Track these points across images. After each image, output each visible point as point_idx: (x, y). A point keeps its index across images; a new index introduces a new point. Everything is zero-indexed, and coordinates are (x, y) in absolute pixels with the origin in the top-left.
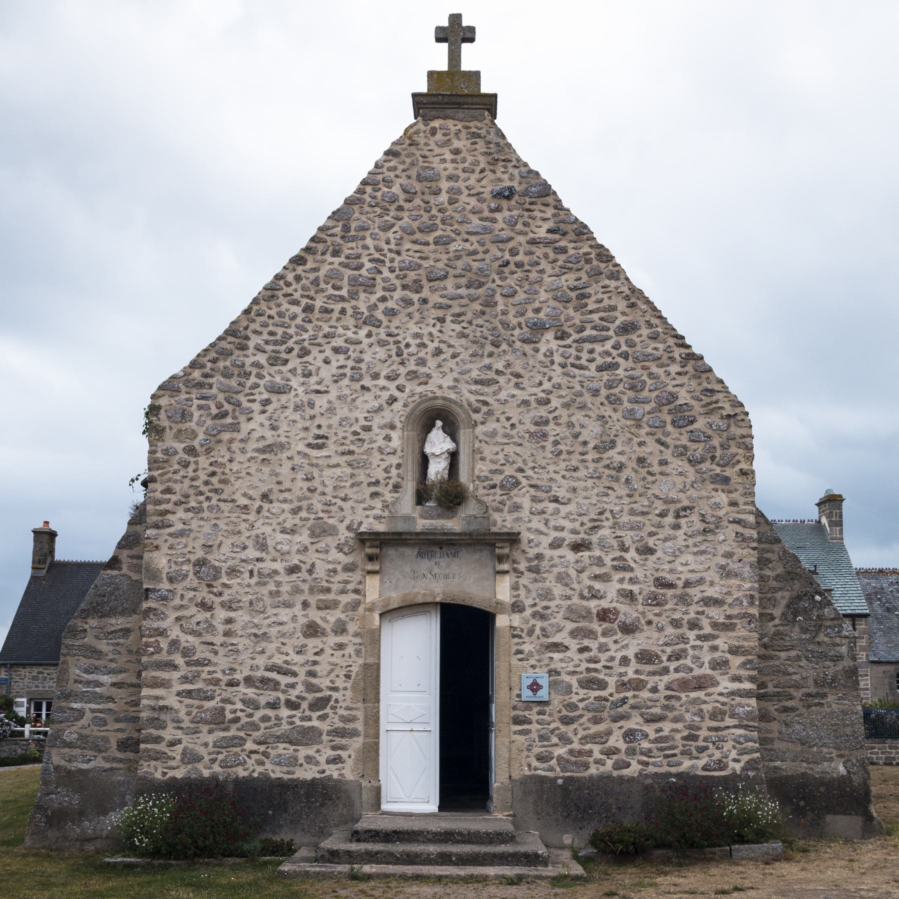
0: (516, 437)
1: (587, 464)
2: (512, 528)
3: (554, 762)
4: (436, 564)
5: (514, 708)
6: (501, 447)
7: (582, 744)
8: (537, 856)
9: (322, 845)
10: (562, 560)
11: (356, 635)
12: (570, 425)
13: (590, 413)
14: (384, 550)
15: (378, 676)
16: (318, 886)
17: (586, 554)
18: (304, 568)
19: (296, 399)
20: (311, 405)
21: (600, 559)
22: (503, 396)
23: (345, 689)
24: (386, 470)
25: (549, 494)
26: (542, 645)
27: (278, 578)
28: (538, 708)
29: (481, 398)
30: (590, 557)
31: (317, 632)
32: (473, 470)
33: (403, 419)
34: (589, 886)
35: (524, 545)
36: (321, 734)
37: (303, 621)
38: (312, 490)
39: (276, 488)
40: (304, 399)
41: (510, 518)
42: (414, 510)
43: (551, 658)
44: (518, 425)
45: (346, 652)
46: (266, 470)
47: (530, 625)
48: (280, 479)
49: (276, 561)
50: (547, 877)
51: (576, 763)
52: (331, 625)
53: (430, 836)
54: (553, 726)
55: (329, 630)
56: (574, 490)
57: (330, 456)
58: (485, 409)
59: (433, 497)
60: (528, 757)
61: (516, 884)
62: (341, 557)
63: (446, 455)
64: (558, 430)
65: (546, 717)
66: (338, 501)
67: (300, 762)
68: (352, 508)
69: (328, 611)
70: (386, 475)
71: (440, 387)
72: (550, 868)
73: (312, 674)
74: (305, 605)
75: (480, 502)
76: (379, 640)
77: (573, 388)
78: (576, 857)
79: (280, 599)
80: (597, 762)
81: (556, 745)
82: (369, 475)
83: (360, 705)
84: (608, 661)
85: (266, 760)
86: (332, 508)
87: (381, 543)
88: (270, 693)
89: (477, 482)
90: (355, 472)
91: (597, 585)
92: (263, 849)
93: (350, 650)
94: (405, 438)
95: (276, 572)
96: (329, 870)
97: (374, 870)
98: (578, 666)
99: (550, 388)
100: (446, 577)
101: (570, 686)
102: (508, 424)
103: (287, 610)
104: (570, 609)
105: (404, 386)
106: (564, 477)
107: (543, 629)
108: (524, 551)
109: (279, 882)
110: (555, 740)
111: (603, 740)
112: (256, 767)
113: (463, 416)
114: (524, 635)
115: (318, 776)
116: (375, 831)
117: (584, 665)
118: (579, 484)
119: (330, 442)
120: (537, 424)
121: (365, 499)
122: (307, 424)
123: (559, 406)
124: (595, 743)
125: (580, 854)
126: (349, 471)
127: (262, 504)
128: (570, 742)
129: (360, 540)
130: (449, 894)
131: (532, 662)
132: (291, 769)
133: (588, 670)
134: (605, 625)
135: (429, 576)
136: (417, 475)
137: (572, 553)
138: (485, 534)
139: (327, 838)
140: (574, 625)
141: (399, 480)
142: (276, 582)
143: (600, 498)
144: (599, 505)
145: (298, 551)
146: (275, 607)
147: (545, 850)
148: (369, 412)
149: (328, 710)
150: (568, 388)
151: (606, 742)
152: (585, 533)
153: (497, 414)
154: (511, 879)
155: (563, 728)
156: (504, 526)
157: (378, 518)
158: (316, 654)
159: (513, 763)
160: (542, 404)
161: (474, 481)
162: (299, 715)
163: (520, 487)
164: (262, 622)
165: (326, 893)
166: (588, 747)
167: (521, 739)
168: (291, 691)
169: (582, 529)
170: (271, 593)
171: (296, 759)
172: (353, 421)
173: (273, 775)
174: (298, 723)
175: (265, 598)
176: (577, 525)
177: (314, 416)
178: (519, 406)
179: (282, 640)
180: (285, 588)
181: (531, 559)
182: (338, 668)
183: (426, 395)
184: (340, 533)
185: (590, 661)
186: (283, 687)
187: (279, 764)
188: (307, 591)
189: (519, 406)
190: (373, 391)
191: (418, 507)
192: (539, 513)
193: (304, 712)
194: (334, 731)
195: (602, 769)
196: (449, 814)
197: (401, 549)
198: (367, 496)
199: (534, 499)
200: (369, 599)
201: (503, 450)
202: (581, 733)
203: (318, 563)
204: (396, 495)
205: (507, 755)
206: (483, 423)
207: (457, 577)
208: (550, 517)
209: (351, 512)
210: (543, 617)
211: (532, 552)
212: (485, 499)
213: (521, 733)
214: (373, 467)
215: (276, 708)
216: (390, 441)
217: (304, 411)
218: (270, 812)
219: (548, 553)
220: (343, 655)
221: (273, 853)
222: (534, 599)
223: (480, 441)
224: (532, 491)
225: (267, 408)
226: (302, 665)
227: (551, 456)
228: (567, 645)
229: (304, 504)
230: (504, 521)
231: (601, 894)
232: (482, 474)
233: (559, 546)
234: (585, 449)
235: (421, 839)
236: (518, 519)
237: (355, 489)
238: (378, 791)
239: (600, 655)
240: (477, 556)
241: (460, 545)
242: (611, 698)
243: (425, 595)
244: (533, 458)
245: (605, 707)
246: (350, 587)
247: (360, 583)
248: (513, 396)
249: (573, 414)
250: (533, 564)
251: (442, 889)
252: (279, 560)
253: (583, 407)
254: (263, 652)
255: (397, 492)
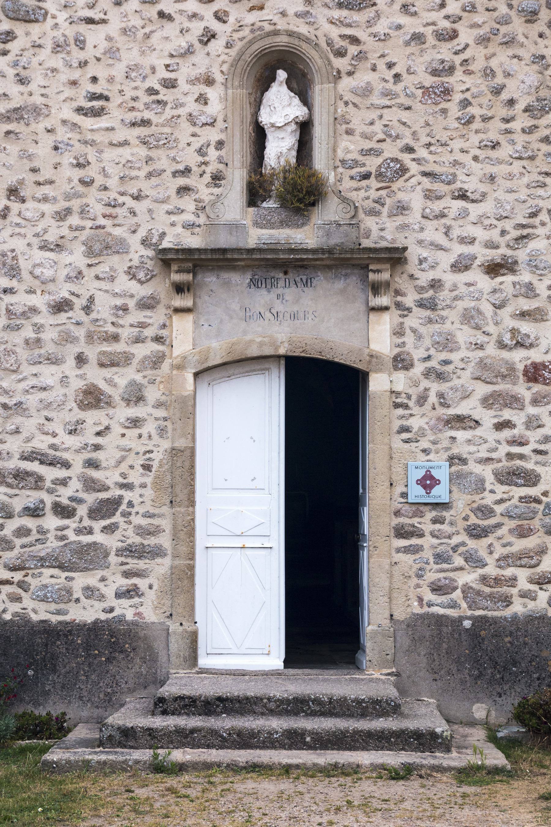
0: (402, 95)
1: (513, 137)
2: (394, 241)
3: (457, 595)
4: (278, 296)
5: (397, 513)
6: (378, 112)
7: (500, 567)
8: (433, 735)
9: (110, 720)
10: (471, 289)
11: (159, 405)
12: (489, 73)
13: (521, 52)
14: (199, 277)
15: (193, 466)
16: (104, 782)
17: (509, 279)
18: (78, 303)
19: (55, 33)
20: (80, 43)
21: (530, 286)
22: (381, 27)
23: (143, 486)
24: (201, 152)
25: (453, 187)
26: (439, 419)
27: (37, 319)
28: (434, 514)
29: (348, 31)
30: (514, 284)
31: (99, 400)
32: (335, 151)
33: (225, 68)
34: (516, 784)
35: (412, 267)
36: (107, 555)
37: (77, 384)
38: (86, 183)
39: (31, 178)
40: (67, 33)
41: (391, 225)
42: (244, 213)
43: (453, 439)
44: (405, 75)
45: (144, 431)
46: (13, 148)
47: (421, 388)
48: (36, 164)
49: (34, 292)
50: (449, 769)
51: (491, 596)
52: (121, 391)
53: (272, 705)
54: (455, 540)
55: (117, 398)
56: (492, 178)
57: (113, 129)
58: (353, 50)
59: (274, 193)
60: (418, 586)
61: (402, 778)
62: (133, 287)
63: (293, 127)
64: (469, 81)
65: (445, 528)
66: (127, 200)
67: (75, 596)
68: (150, 211)
69: (115, 369)
70: (200, 159)
71: (283, 14)
72: (454, 754)
73: (92, 464)
74: (81, 360)
75: (345, 200)
76: (194, 413)
77: (494, 10)
78: (493, 739)
79: (42, 351)
80: (523, 595)
81: (462, 569)
82: (174, 159)
83: (166, 510)
84: (540, 442)
85: (23, 594)
86: (118, 210)
87: (195, 266)
88: (28, 492)
89: (340, 170)
90: (153, 153)
91: (525, 327)
92: (19, 729)
93: (150, 427)
94: (230, 98)
95: (34, 310)
96: (121, 758)
97: (188, 757)
98: (495, 450)
99: (458, 12)
100: (294, 316)
101: (482, 481)
102: (389, 75)
103: (53, 368)
104: (482, 364)
105: (226, 13)
106: (476, 158)
107: (441, 396)
108: (411, 276)
109: (45, 778)
110: (459, 561)
111: (533, 562)
112: (8, 604)
113: (319, 61)
114: (411, 404)
115: (103, 617)
116: (190, 698)
117: (504, 449)
118: (500, 170)
119: (111, 106)
120: (435, 73)
121: (169, 197)
122: (76, 75)
123: (471, 42)
124: (521, 566)
125: (500, 735)
126: (143, 152)
127: (9, 203)
128: (482, 564)
129: (162, 260)
130: (301, 794)
131: (424, 444)
132: (62, 606)
133: (510, 456)
134: (537, 388)
135: (268, 315)
136: (248, 159)
137: (487, 277)
138: (352, 251)
139: (117, 710)
140: (489, 389)
141: (221, 167)
142: (35, 325)
143: (533, 191)
144: (531, 202)
145: (68, 278)
146: (35, 364)
147: (446, 727)
148: (172, 56)
149: (117, 518)
150: (488, 10)
151: (537, 565)
152: (508, 246)
153: (373, 58)
154: (396, 771)
155: (472, 544)
156: (382, 238)
157: (189, 226)
158: (98, 434)
159: (395, 595)
160: (445, 40)
161: (336, 168)
162: (74, 525)
163: (407, 175)
164: (15, 386)
165: (116, 794)
166: (509, 572)
167: (407, 559)
168: (61, 490)
169: (502, 241)
170: (27, 342)
171: (69, 592)
172: (148, 71)
173: (35, 618)
174: (72, 537)
175: (18, 350)
176: (495, 235)
177: (86, 63)
178: (407, 44)
179: (46, 413)
180: (48, 335)
181: (422, 288)
182: (133, 455)
183: (261, 28)
184: (132, 249)
185: (512, 442)
186: (48, 484)
187: (44, 599)
188: (82, 339)
189: (407, 44)
190: (177, 21)
191: (251, 210)
192: (436, 217)
193: (81, 520)
194: (126, 549)
195: (531, 605)
196: (299, 671)
197: (226, 275)
198: (172, 192)
199: (429, 195)
200: (177, 352)
201: (381, 117)
202: (499, 551)
203: (99, 297)
204: (216, 191)
205: (387, 584)
206: (350, 74)
207: (310, 316)
208: (453, 223)
209: (148, 217)
210: (440, 377)
211: (424, 278)
212: (353, 195)
213: (407, 550)
214: (180, 146)
215: (38, 516)
216: (206, 103)
217: (68, 53)
218: (30, 673)
219: (449, 278)
220: (140, 436)
221: (35, 735)
222: (428, 350)
223: (346, 103)
224: (426, 182)
225: (8, 46)
226: (78, 451)
227: (457, 125)
228: (477, 418)
229: (75, 204)
230: (382, 230)
231: (536, 795)
232: (349, 156)
233: (467, 268)
234: (511, 113)
235: (258, 709)
236: (404, 227)
237: (154, 181)
238: (193, 638)
239: (528, 433)
240: (340, 284)
241: (315, 267)
242: (544, 499)
243: (261, 344)
244: (427, 130)
245: (535, 513)
246: (149, 332)
247: (164, 326)
248: (399, 27)
249: (494, 55)
250: (426, 295)
251: (292, 786)
252: (39, 292)
253: (509, 43)
254: (17, 431)
255: (217, 186)
